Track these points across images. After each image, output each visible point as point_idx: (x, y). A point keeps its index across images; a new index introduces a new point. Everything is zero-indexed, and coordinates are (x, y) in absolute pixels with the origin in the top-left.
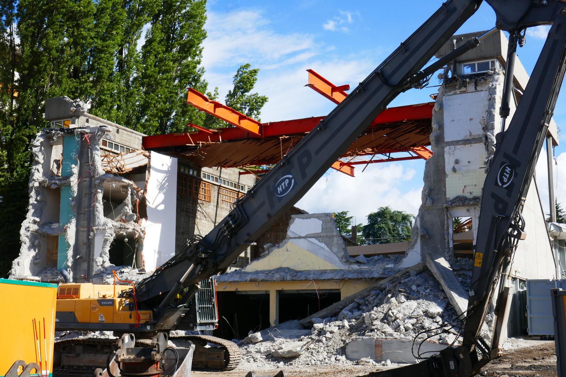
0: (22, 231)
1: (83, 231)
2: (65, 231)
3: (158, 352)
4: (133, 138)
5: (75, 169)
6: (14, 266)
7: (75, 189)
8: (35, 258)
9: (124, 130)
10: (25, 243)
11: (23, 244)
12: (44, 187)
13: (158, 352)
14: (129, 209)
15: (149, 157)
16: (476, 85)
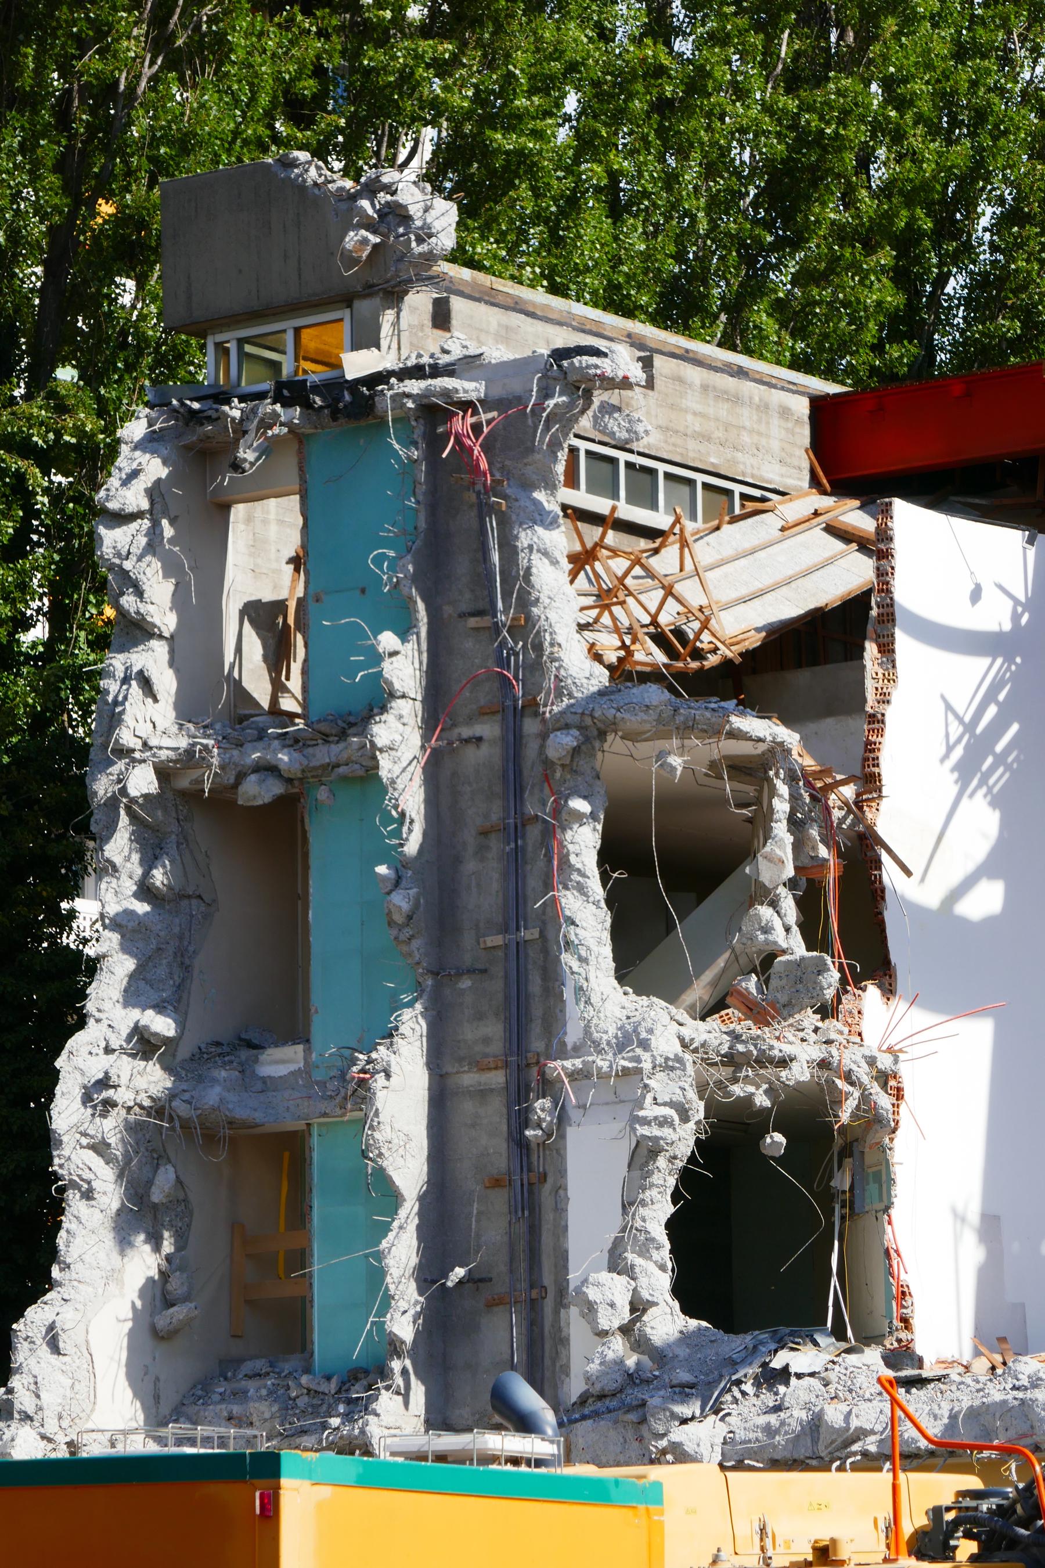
0: (66, 1113)
1: (483, 1094)
2: (361, 1093)
4: (746, 416)
5: (404, 665)
6: (21, 1355)
7: (411, 798)
8: (159, 1294)
10: (88, 1195)
11: (74, 1202)
12: (192, 796)
14: (780, 925)
15: (878, 547)
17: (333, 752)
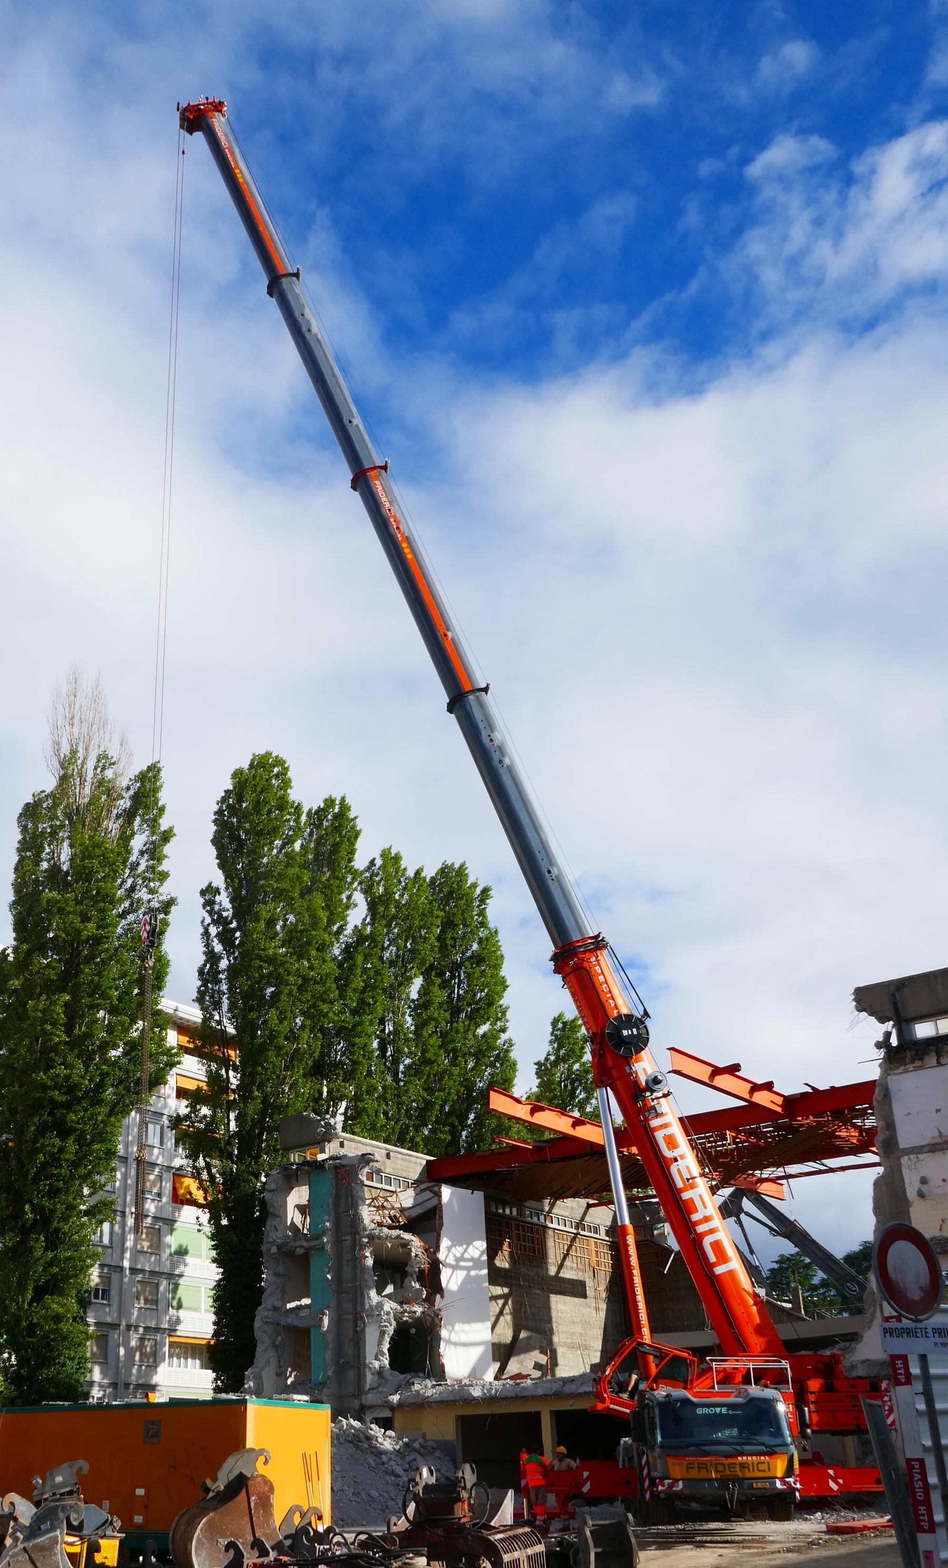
0: (257, 1324)
3: (464, 1488)
9: (398, 1152)
13: (464, 1488)
16: (939, 1057)
17: (316, 1243)
